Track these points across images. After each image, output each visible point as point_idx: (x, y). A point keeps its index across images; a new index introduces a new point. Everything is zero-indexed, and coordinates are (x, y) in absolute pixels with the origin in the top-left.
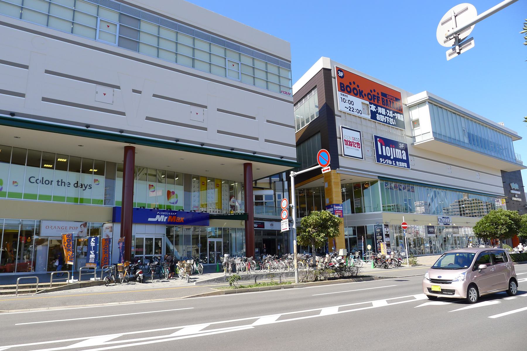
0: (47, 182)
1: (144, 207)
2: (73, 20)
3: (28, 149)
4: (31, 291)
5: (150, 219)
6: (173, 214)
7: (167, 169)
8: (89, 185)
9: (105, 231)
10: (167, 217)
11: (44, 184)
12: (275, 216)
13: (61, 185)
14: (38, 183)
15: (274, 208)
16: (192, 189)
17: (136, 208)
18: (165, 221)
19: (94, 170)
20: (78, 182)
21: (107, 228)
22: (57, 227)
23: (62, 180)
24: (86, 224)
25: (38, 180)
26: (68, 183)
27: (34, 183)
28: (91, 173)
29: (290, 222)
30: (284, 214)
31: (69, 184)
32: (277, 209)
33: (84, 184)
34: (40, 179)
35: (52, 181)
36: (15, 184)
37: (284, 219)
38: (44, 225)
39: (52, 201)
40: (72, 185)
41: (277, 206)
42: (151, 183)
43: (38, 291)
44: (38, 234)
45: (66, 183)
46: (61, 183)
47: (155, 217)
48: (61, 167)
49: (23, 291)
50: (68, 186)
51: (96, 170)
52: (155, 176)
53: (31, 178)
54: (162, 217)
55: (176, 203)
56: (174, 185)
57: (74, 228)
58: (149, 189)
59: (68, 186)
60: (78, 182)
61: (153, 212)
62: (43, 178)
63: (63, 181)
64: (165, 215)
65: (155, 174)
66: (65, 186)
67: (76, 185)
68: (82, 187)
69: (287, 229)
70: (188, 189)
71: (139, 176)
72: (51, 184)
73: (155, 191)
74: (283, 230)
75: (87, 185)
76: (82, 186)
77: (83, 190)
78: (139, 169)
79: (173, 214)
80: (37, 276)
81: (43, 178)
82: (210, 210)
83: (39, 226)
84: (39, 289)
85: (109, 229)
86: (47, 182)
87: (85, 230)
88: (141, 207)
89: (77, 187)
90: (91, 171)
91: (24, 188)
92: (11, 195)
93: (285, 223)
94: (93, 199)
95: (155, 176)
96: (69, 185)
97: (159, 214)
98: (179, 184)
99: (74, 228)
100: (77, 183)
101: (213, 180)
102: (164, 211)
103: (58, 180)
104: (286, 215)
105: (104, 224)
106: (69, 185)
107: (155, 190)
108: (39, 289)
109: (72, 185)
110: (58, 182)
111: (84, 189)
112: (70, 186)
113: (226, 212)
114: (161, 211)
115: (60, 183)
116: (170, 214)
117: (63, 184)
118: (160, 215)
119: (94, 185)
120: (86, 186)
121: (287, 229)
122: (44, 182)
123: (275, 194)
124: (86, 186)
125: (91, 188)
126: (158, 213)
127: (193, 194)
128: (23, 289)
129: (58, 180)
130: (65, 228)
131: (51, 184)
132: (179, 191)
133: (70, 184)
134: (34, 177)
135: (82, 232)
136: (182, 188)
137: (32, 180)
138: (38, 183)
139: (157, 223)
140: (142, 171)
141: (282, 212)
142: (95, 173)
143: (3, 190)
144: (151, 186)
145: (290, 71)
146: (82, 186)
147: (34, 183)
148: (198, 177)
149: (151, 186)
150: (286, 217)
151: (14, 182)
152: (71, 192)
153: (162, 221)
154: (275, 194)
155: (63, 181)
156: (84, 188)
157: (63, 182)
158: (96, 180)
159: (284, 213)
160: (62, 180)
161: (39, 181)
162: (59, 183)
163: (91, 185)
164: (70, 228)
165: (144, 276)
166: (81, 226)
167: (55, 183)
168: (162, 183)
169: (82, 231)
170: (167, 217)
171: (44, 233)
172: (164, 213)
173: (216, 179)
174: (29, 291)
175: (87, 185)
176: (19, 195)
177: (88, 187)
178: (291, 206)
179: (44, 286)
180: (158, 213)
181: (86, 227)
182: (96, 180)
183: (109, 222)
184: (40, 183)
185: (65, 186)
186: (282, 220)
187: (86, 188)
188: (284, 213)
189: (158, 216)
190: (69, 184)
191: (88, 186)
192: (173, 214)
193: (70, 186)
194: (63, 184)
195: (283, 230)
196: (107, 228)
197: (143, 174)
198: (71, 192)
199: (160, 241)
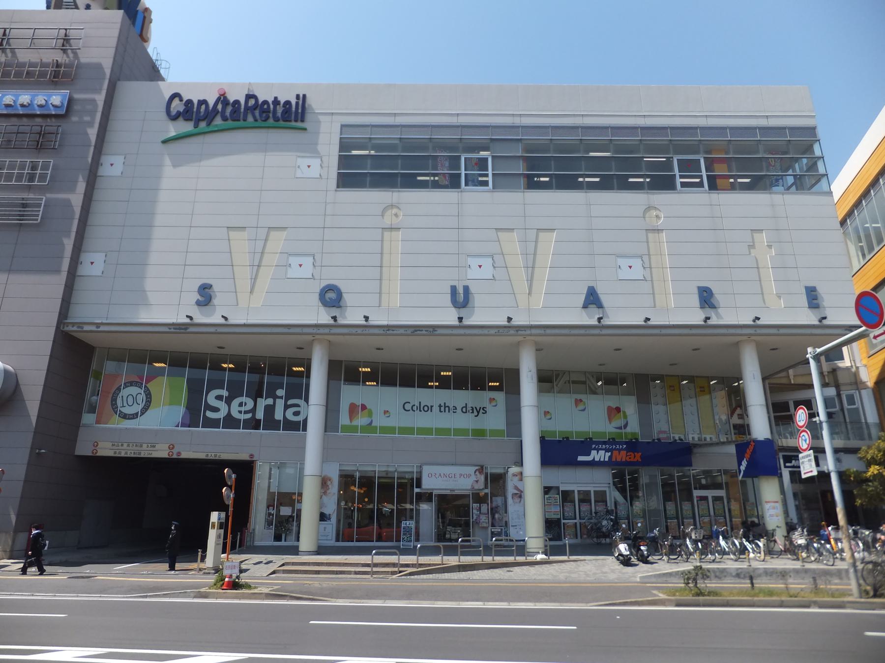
0: (426, 409)
1: (567, 438)
2: (54, 133)
3: (452, 365)
4: (391, 572)
5: (580, 458)
6: (621, 447)
7: (602, 369)
8: (484, 408)
9: (512, 480)
10: (610, 453)
11: (423, 411)
12: (848, 442)
13: (445, 411)
14: (415, 411)
15: (843, 426)
16: (653, 400)
17: (624, 440)
18: (607, 459)
19: (432, 384)
20: (466, 404)
21: (515, 475)
22: (442, 475)
23: (445, 403)
24: (483, 469)
25: (414, 407)
26: (453, 407)
27: (409, 410)
28: (431, 387)
29: (819, 451)
30: (802, 439)
31: (454, 408)
32: (849, 427)
33: (476, 408)
34: (417, 404)
35: (432, 406)
36: (387, 415)
37: (805, 450)
38: (426, 470)
39: (359, 434)
40: (459, 410)
41: (848, 420)
42: (579, 397)
43: (400, 572)
44: (419, 485)
45: (451, 407)
46: (444, 408)
47: (589, 454)
48: (445, 384)
49: (382, 572)
50: (453, 412)
51: (437, 384)
52: (584, 383)
53: (406, 405)
54: (602, 453)
55: (626, 426)
56: (570, 395)
57: (465, 476)
58: (576, 407)
59: (453, 412)
60: (466, 404)
61: (587, 444)
62: (420, 403)
63: (446, 405)
64: (607, 450)
65: (584, 379)
66: (449, 412)
67: (464, 410)
68: (473, 412)
69: (811, 471)
70: (644, 399)
71: (558, 386)
72: (431, 411)
73: (586, 410)
74: (805, 473)
75: (480, 408)
76: (473, 410)
77: (475, 416)
78: (557, 376)
79: (619, 447)
80: (397, 549)
81: (420, 403)
82: (693, 436)
83: (420, 473)
84: (401, 569)
85: (517, 476)
86: (426, 409)
87: (482, 478)
88: (563, 438)
89: (466, 412)
90: (431, 385)
91: (398, 420)
92: (385, 430)
93: (806, 459)
94: (455, 427)
95: (584, 383)
96: (455, 411)
97: (595, 449)
98: (629, 394)
99: (465, 476)
100: (466, 407)
101: (691, 379)
102: (604, 443)
103: (440, 404)
104: (808, 442)
105: (508, 468)
106: (455, 411)
107: (585, 408)
108: (401, 569)
109: (459, 410)
110: (440, 406)
111: (476, 414)
112: (456, 412)
113: (727, 438)
114: (598, 443)
115: (442, 409)
116: (614, 446)
117: (447, 409)
118: (598, 450)
119: (489, 408)
120: (478, 410)
121: (811, 471)
122: (422, 409)
123: (839, 395)
124: (478, 410)
125: (486, 412)
126: (594, 446)
127: (654, 408)
128: (385, 568)
129: (440, 404)
130: (453, 477)
131: (431, 411)
132: (630, 406)
133: (456, 409)
134: (409, 403)
135: (477, 481)
136: (633, 399)
137: (408, 407)
138: (415, 411)
139: (593, 464)
140: (562, 377)
141: (800, 436)
142: (437, 387)
143: (373, 424)
144: (578, 402)
145: (817, 140)
146: (473, 410)
147: (409, 410)
148: (661, 377)
149: (578, 402)
150: (809, 445)
151: (386, 412)
152: (466, 422)
153: (602, 460)
154: (839, 395)
155: (446, 405)
156: (476, 413)
157: (447, 407)
158: (492, 400)
159: (803, 438)
160: (445, 403)
161: (415, 408)
162: (441, 408)
163: (486, 408)
164: (461, 475)
165: (648, 553)
166: (475, 472)
167: (436, 409)
168: (597, 394)
169: (478, 481)
170: (610, 453)
171: (430, 483)
172: (603, 446)
173: (666, 376)
174: (388, 572)
175: (480, 408)
176: (391, 430)
177: (482, 411)
178: (818, 422)
179: (411, 566)
180: (594, 446)
181: (483, 473)
182: (492, 400)
183: (516, 465)
184: (417, 410)
185: (449, 412)
186: (802, 453)
187: (478, 412)
188: (803, 438)
189: (594, 453)
190: (454, 408)
191: (481, 409)
192: (619, 447)
193: (456, 412)
194: (447, 409)
195: (805, 473)
196: (514, 475)
197: (565, 383)
198: (466, 422)
199: (673, 494)
